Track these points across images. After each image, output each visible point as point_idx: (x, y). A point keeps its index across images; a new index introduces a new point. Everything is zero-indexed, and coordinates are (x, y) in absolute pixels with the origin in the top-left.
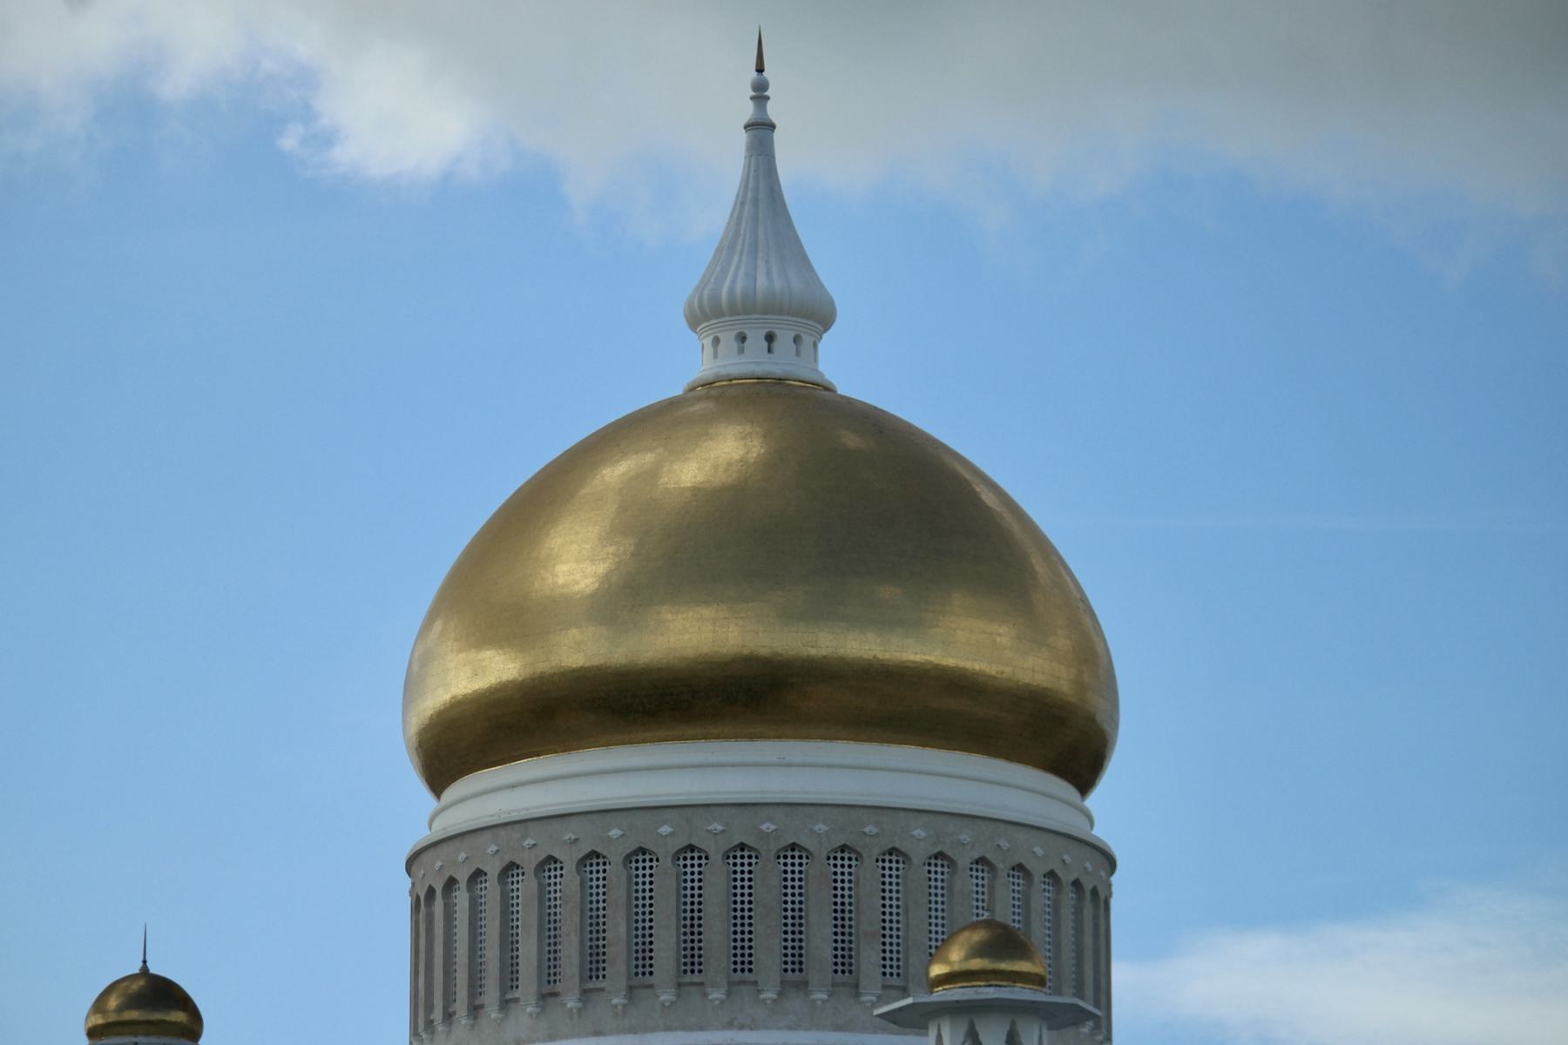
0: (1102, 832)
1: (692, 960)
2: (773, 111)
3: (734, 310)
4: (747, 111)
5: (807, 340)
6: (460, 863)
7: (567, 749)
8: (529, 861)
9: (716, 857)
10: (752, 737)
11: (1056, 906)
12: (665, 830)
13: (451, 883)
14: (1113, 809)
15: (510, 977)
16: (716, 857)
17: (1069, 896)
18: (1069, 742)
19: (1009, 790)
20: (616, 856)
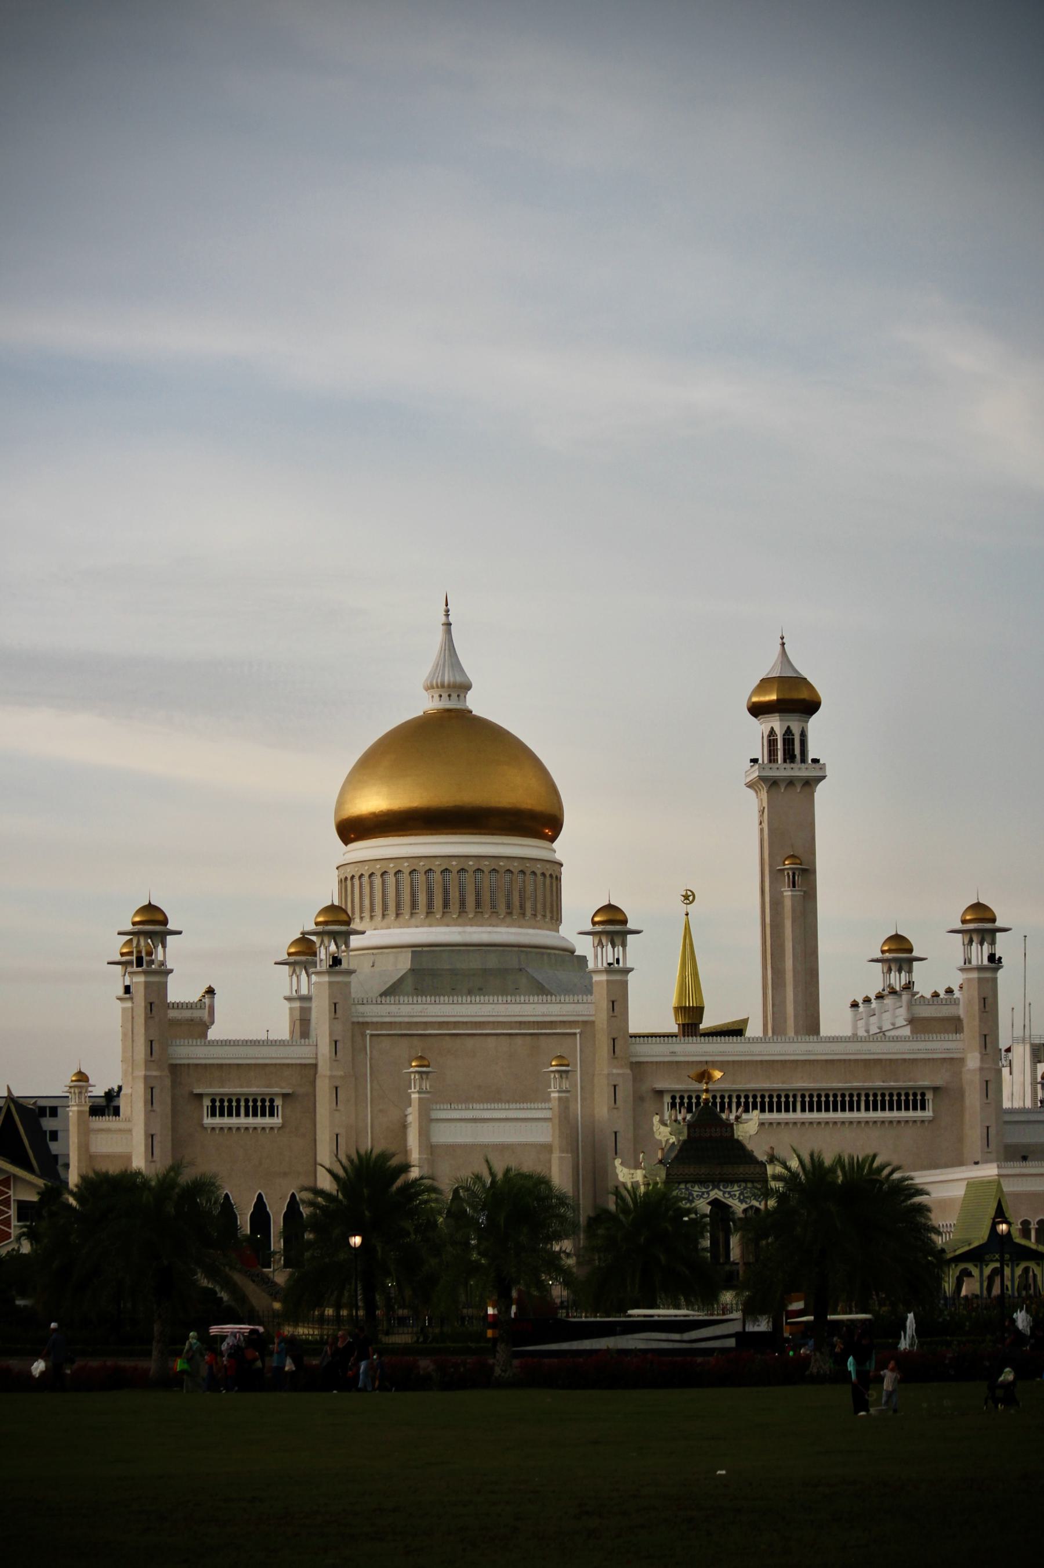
0: (558, 856)
1: (478, 904)
2: (451, 619)
3: (449, 686)
4: (443, 619)
5: (462, 696)
6: (349, 871)
7: (493, 834)
9: (486, 872)
10: (447, 834)
11: (551, 883)
12: (471, 863)
13: (353, 877)
14: (562, 848)
15: (385, 907)
16: (486, 872)
17: (540, 878)
18: (545, 823)
20: (455, 870)
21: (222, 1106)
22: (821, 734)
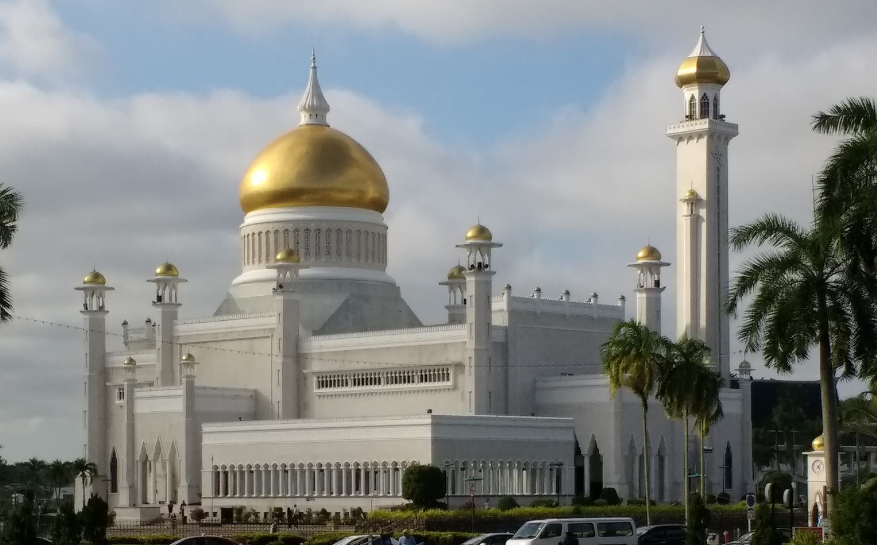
19: (366, 215)
22: (730, 100)
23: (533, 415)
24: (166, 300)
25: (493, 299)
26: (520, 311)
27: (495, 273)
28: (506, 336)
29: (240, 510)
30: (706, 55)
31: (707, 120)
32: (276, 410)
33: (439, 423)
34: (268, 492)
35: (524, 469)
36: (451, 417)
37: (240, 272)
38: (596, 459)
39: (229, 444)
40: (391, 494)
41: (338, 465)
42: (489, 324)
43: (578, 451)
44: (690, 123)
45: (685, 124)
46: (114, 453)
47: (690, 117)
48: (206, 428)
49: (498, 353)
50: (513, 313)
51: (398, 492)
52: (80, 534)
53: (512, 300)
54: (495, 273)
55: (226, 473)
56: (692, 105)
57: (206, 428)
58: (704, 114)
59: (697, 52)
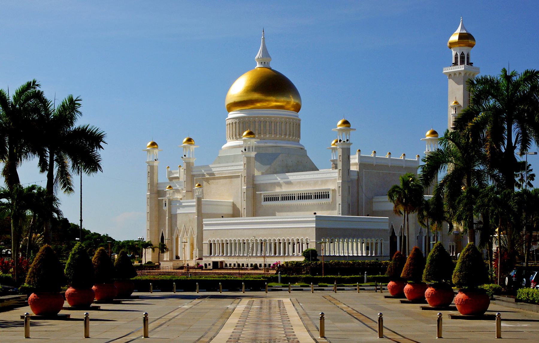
8: (234, 122)
21: (267, 199)
23: (368, 216)
24: (187, 156)
25: (351, 157)
26: (363, 164)
27: (352, 144)
28: (358, 175)
29: (222, 262)
30: (463, 32)
31: (463, 65)
32: (243, 212)
33: (319, 219)
34: (275, 254)
35: (332, 242)
36: (151, 213)
37: (226, 142)
38: (404, 239)
39: (217, 230)
40: (254, 255)
41: (235, 240)
42: (349, 169)
43: (393, 233)
44: (455, 67)
45: (453, 67)
46: (162, 234)
47: (456, 64)
48: (205, 221)
49: (352, 184)
50: (362, 165)
51: (81, 251)
52: (340, 275)
53: (360, 158)
54: (352, 144)
55: (231, 244)
56: (456, 58)
57: (205, 221)
58: (462, 62)
59: (458, 31)
